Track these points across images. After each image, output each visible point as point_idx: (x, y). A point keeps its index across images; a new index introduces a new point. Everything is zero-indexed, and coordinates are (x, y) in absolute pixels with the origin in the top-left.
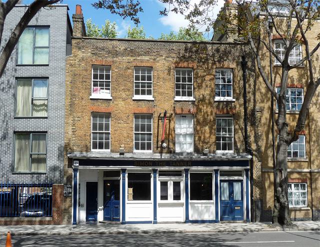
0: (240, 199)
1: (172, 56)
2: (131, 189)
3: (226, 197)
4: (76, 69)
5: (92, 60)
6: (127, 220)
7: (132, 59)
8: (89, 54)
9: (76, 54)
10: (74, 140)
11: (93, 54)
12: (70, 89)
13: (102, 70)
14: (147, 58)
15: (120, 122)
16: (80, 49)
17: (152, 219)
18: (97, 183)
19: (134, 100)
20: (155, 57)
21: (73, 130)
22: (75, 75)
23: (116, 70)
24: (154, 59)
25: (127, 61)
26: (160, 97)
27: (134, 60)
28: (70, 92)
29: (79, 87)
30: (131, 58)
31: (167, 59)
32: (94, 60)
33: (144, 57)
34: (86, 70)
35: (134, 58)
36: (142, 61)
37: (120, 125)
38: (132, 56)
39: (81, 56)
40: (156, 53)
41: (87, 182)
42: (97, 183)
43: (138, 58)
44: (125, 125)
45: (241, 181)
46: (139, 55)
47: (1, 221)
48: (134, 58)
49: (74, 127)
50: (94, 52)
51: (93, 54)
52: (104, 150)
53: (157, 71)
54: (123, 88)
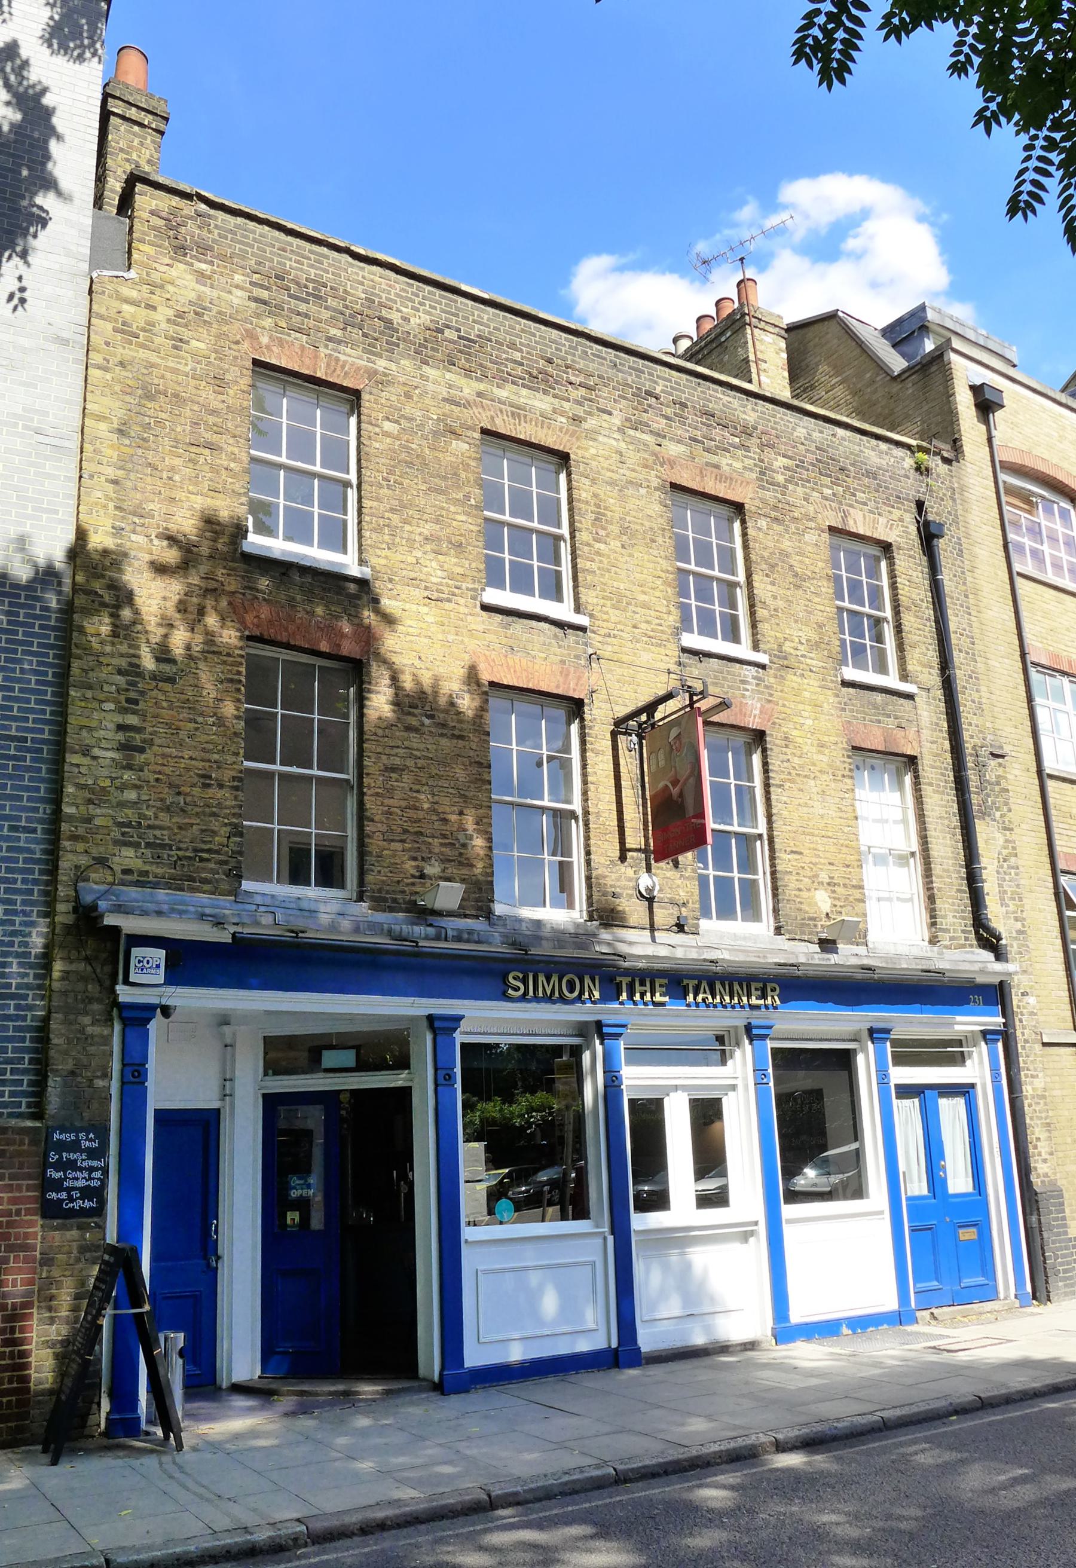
0: (969, 1188)
1: (655, 426)
2: (479, 1147)
3: (916, 1185)
4: (154, 358)
5: (251, 336)
6: (474, 1357)
7: (469, 388)
8: (238, 298)
9: (156, 277)
10: (134, 804)
11: (257, 300)
12: (111, 472)
13: (963, 43)
14: (541, 403)
15: (413, 721)
16: (180, 250)
17: (797, 1315)
18: (215, 1115)
19: (485, 608)
20: (580, 411)
21: (120, 736)
22: (149, 396)
23: (388, 426)
24: (576, 420)
25: (444, 392)
26: (614, 615)
27: (479, 394)
28: (111, 487)
29: (172, 469)
30: (462, 381)
31: (632, 432)
32: (265, 340)
33: (524, 392)
34: (220, 383)
35: (482, 386)
36: (518, 412)
37: (414, 740)
38: (468, 372)
39: (192, 296)
40: (582, 391)
41: (264, 1096)
42: (215, 1115)
43: (496, 390)
44: (444, 742)
45: (965, 1091)
46: (503, 379)
47: (3, 1378)
48: (482, 386)
49: (132, 720)
50: (264, 294)
51: (257, 300)
52: (311, 893)
53: (594, 481)
54: (427, 529)
